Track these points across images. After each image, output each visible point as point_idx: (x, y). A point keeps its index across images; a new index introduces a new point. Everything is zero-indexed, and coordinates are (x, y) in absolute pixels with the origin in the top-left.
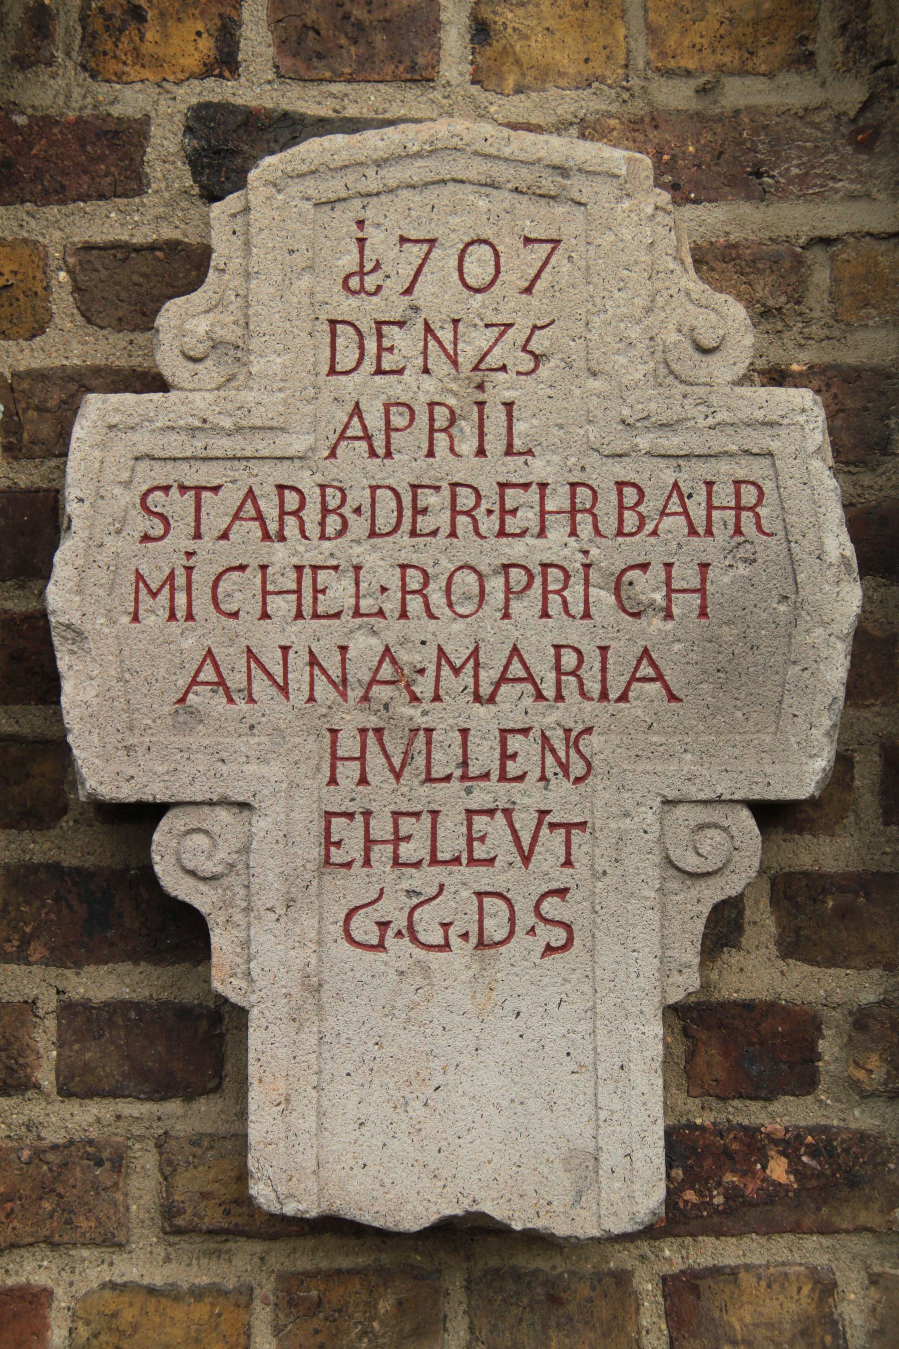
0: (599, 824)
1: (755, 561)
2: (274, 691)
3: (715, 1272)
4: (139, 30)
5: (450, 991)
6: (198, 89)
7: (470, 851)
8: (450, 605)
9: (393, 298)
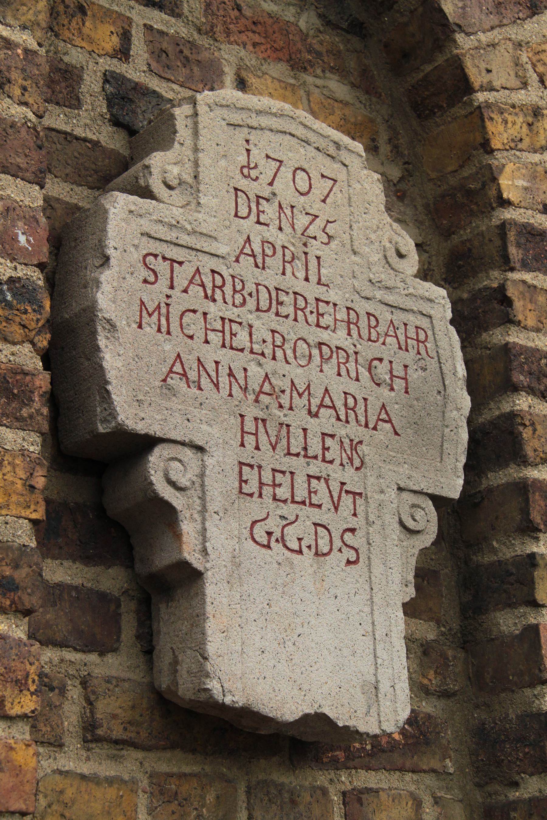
0: (369, 494)
1: (426, 369)
2: (211, 386)
3: (369, 790)
4: (83, 20)
5: (303, 578)
6: (109, 63)
7: (310, 499)
8: (295, 358)
9: (264, 185)
